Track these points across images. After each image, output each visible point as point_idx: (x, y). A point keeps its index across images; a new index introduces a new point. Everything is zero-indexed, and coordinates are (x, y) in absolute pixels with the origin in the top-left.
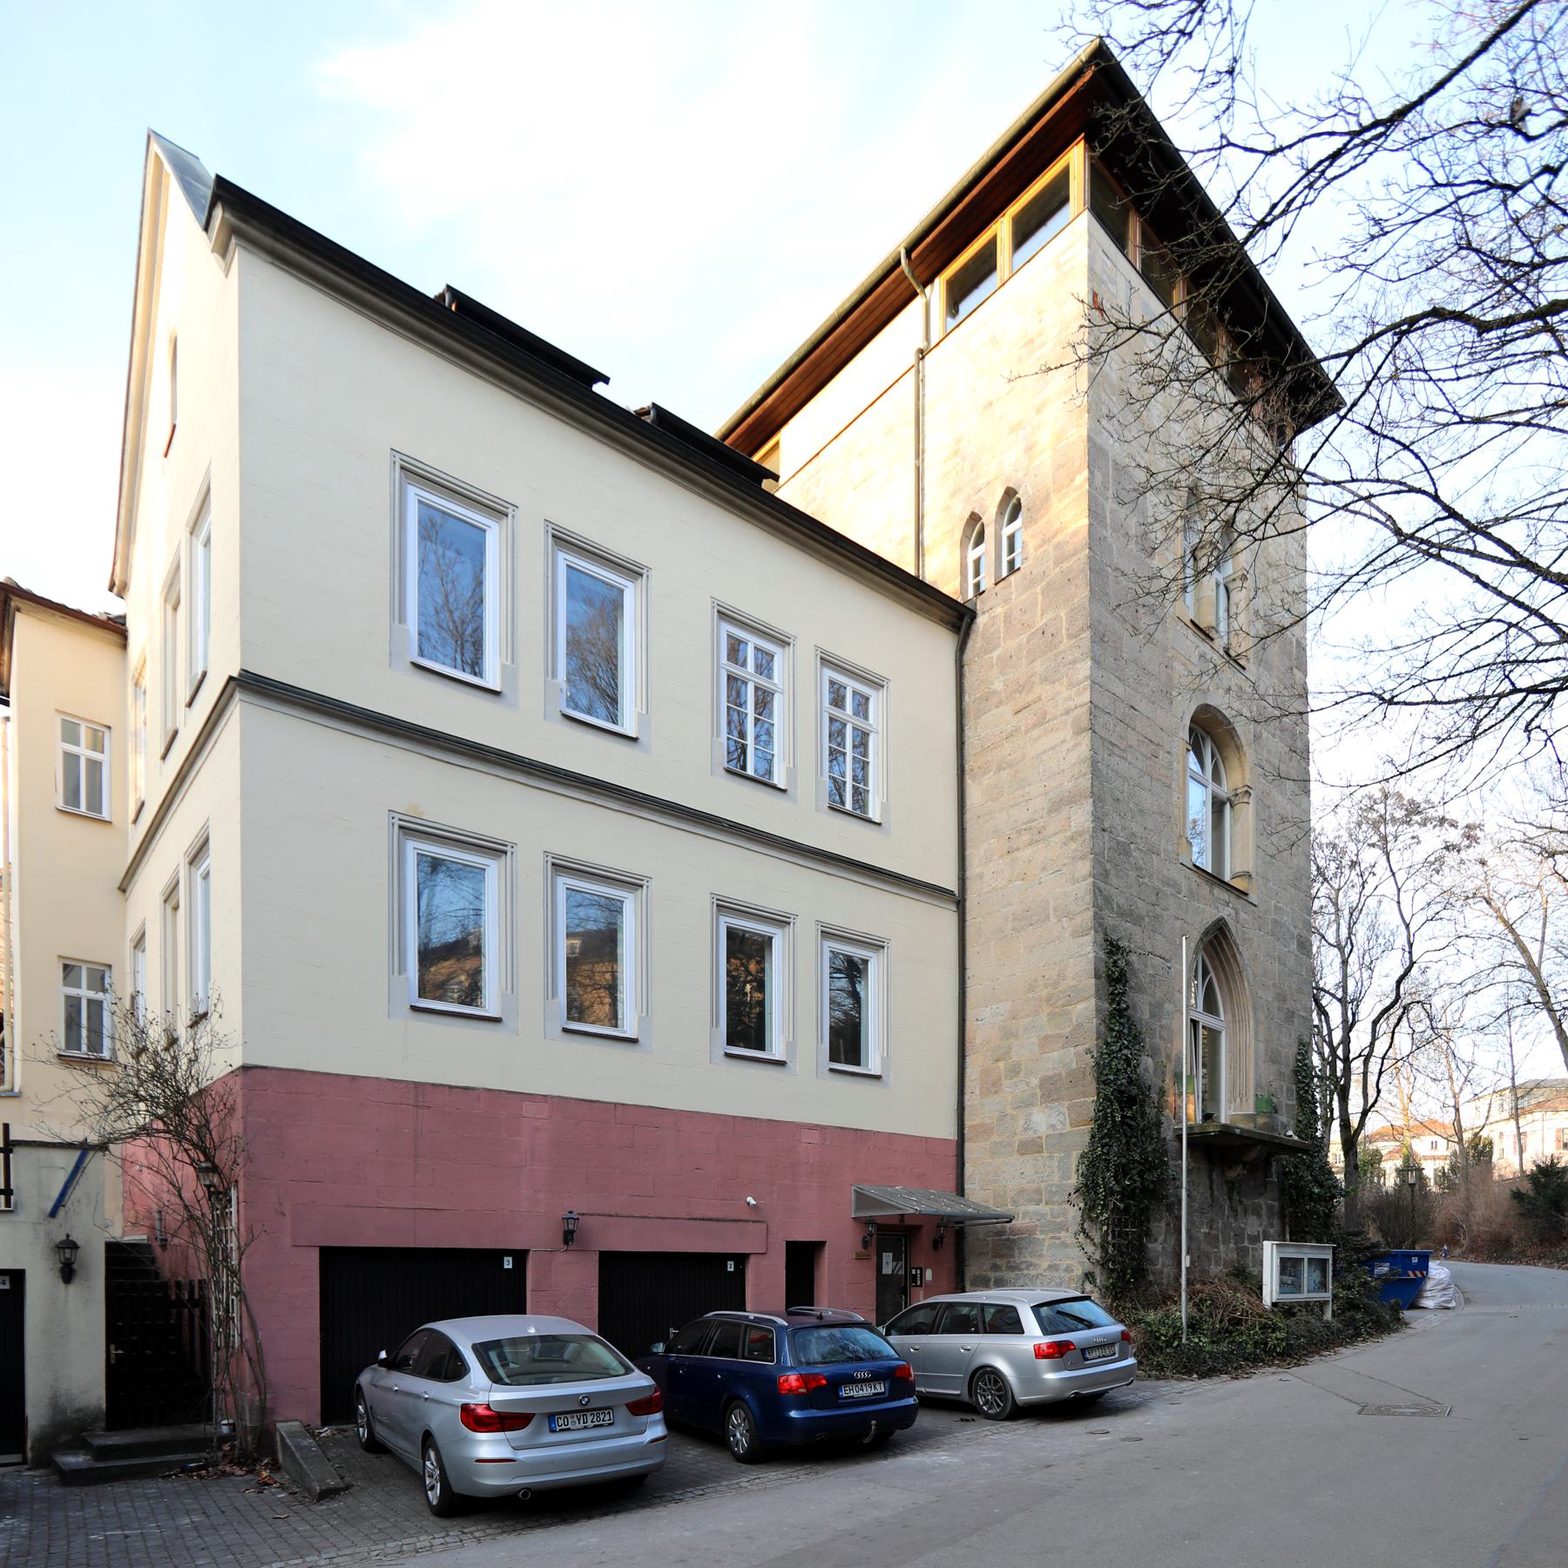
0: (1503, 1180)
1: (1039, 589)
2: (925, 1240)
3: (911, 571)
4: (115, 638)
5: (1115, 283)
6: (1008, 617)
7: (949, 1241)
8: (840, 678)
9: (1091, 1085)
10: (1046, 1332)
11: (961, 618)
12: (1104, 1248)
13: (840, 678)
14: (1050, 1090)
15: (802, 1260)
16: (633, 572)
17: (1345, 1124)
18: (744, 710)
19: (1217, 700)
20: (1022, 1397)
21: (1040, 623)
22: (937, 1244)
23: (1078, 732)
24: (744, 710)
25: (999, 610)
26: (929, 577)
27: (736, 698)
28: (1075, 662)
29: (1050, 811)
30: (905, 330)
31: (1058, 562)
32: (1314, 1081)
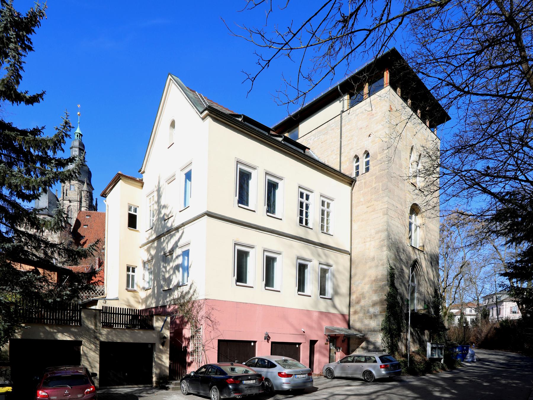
0: (56, 337)
1: (374, 177)
2: (340, 340)
3: (337, 168)
4: (140, 184)
5: (395, 101)
6: (365, 183)
7: (346, 340)
8: (324, 199)
9: (386, 303)
10: (382, 362)
11: (352, 182)
12: (388, 343)
13: (324, 199)
14: (374, 304)
15: (313, 343)
16: (281, 179)
17: (176, 243)
18: (303, 210)
19: (417, 202)
20: (376, 377)
21: (374, 185)
22: (343, 341)
23: (384, 214)
24: (303, 210)
25: (363, 181)
26: (342, 171)
27: (301, 206)
28: (383, 197)
29: (376, 233)
30: (335, 107)
31: (379, 171)
32: (436, 301)
